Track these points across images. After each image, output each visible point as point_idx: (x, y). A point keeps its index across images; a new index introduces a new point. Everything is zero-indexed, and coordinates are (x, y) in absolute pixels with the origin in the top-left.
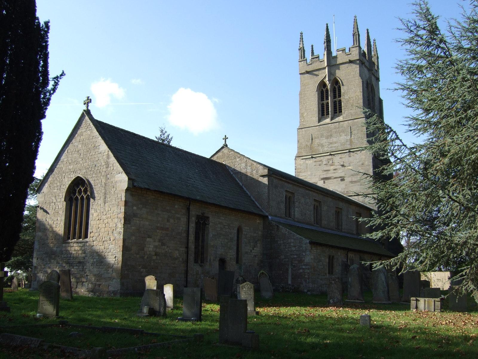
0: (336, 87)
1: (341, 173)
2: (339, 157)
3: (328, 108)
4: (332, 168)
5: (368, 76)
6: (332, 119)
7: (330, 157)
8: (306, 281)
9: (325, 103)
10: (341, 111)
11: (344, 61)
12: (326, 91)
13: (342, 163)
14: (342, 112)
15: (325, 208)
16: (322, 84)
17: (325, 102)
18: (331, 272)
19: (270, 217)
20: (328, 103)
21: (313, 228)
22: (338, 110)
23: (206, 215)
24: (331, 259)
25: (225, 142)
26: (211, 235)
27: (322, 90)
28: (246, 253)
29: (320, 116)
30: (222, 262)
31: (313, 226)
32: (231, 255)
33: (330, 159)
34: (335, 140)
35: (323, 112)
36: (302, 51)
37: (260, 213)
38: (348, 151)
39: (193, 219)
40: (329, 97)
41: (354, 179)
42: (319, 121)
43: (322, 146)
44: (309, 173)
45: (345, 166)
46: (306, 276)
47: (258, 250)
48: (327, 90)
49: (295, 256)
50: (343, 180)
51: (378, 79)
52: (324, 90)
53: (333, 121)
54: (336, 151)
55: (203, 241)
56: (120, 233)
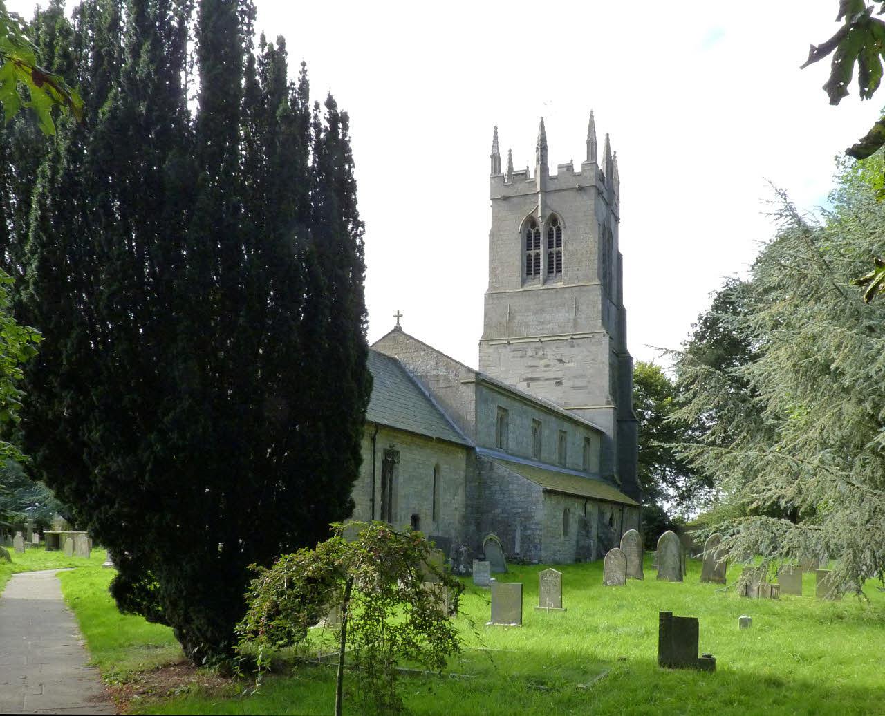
0: (554, 229)
1: (555, 372)
2: (555, 345)
3: (537, 264)
4: (542, 362)
5: (605, 214)
6: (545, 282)
7: (540, 345)
8: (536, 548)
9: (533, 255)
10: (559, 270)
11: (571, 185)
12: (536, 233)
13: (558, 357)
14: (561, 271)
15: (546, 432)
16: (531, 222)
17: (533, 252)
18: (565, 533)
19: (478, 449)
20: (538, 255)
21: (530, 463)
22: (555, 266)
23: (396, 449)
24: (567, 512)
25: (398, 321)
26: (401, 480)
27: (529, 231)
28: (445, 504)
29: (525, 276)
30: (415, 519)
31: (532, 460)
32: (425, 511)
33: (539, 348)
34: (548, 317)
35: (530, 267)
36: (496, 158)
37: (463, 442)
38: (569, 337)
39: (380, 455)
40: (541, 246)
41: (579, 383)
42: (523, 283)
43: (527, 326)
44: (503, 369)
45: (564, 362)
46: (537, 541)
47: (459, 499)
48: (537, 234)
49: (520, 511)
50: (559, 383)
51: (617, 220)
52: (532, 231)
53: (545, 287)
54: (550, 337)
55: (391, 489)
56: (704, 588)
